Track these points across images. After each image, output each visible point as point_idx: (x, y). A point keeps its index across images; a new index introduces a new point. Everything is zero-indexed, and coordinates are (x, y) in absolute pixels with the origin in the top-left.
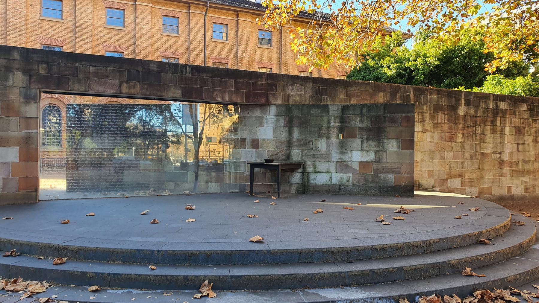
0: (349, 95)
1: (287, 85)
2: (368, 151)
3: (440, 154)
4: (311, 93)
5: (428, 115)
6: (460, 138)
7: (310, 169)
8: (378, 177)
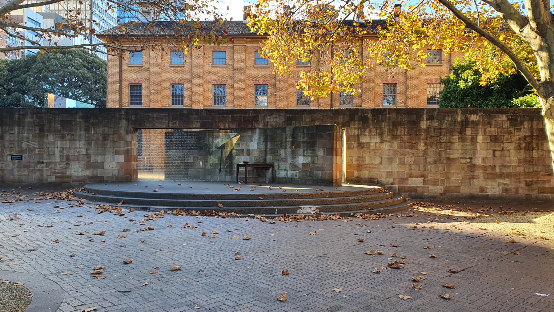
0: (313, 119)
2: (307, 156)
3: (400, 159)
4: (283, 120)
5: (386, 129)
6: (422, 146)
7: (276, 168)
8: (312, 173)
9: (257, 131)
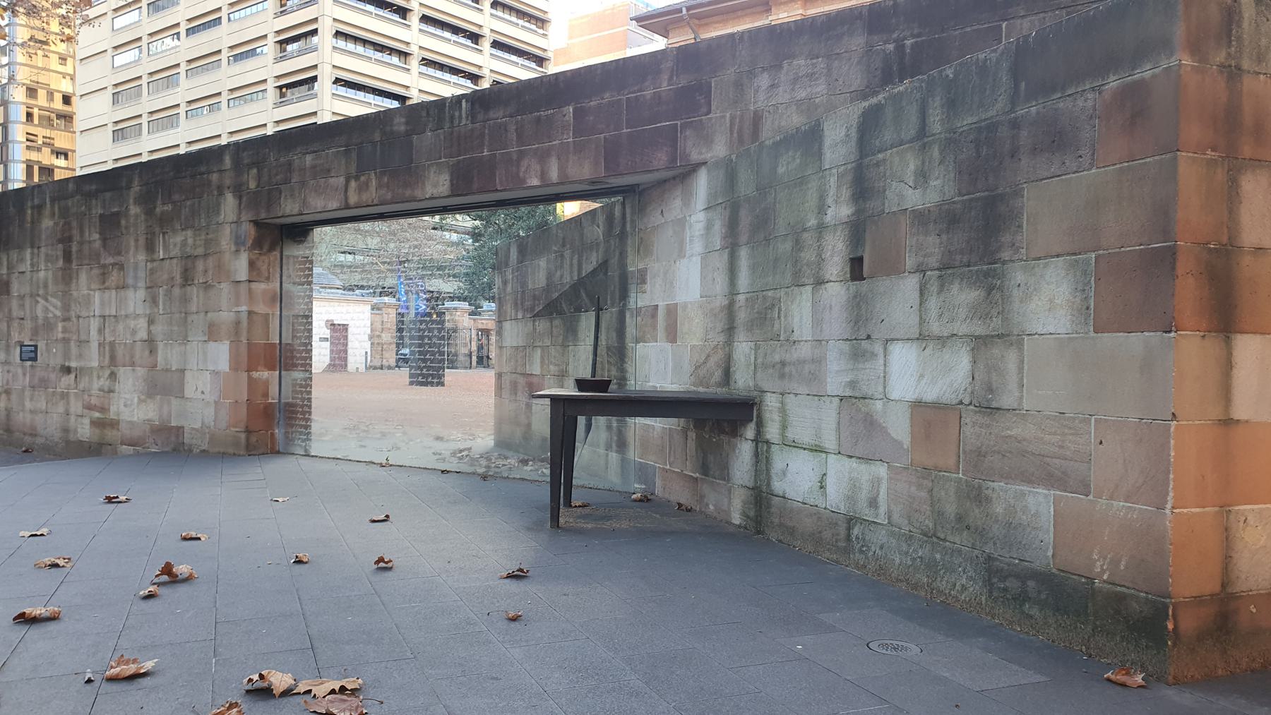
1: (752, 74)
2: (942, 341)
7: (772, 432)
9: (702, 184)
